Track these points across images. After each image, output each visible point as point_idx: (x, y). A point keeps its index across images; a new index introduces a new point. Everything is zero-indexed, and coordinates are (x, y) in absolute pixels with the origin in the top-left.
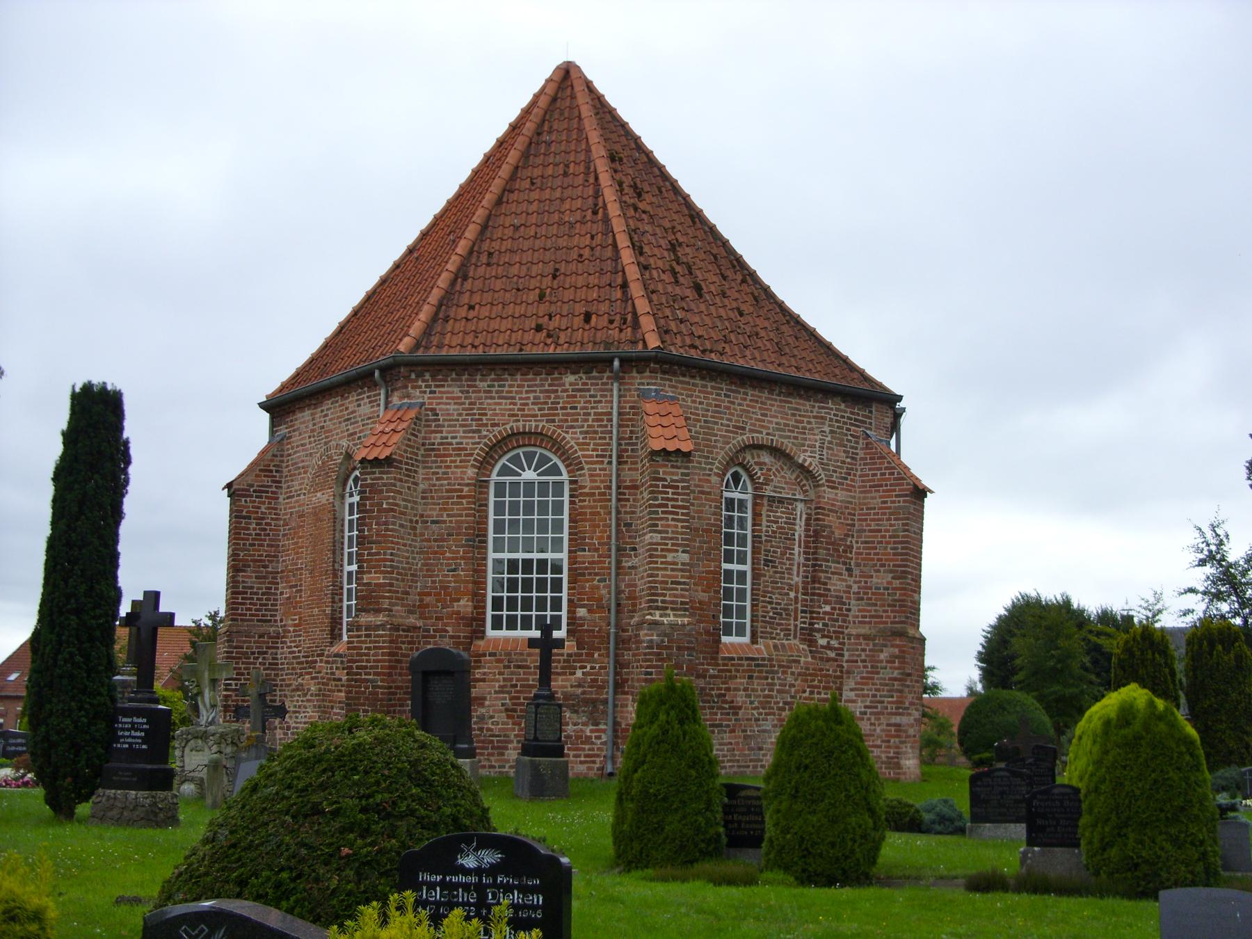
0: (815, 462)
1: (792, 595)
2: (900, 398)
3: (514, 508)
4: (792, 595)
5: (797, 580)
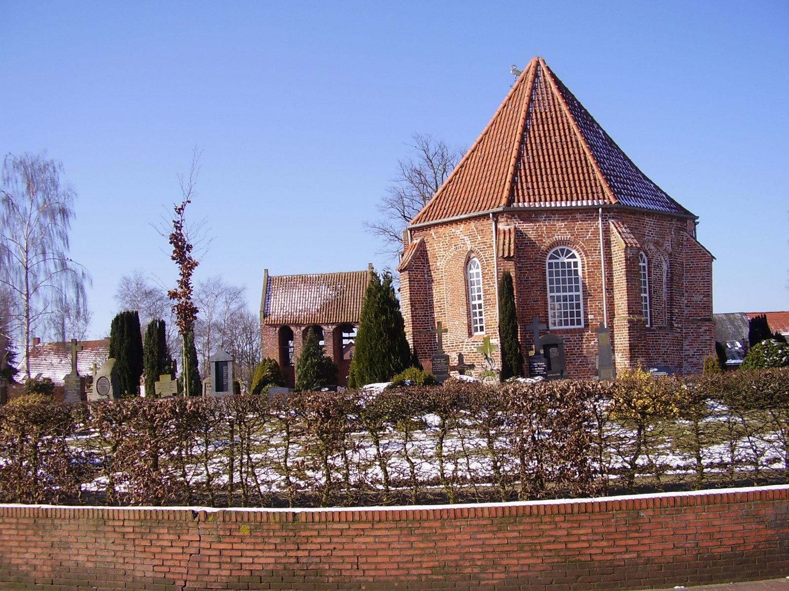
0: (458, 232)
1: (663, 306)
2: (697, 218)
3: (557, 274)
4: (663, 306)
5: (665, 299)
